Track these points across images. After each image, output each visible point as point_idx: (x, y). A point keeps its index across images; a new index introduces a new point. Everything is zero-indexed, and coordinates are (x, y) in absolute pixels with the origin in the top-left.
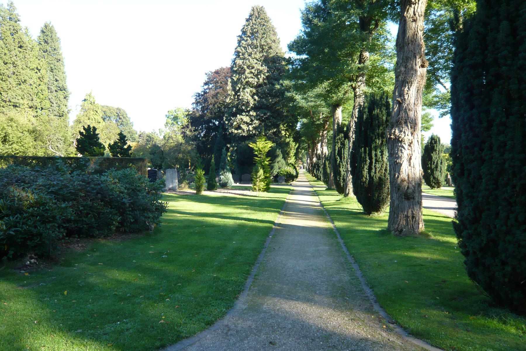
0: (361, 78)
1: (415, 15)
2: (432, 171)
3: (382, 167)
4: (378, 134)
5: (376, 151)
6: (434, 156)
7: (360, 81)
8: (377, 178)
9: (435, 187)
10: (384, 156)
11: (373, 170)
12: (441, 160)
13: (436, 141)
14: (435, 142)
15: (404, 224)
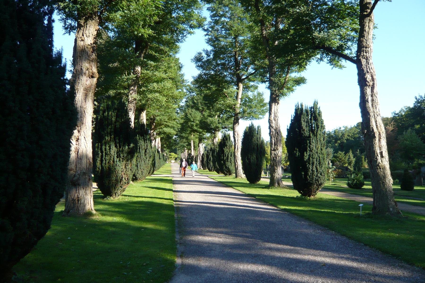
0: (133, 87)
1: (83, 35)
2: (225, 162)
3: (110, 159)
4: (107, 132)
5: (105, 146)
6: (226, 150)
7: (132, 90)
8: (107, 168)
9: (227, 175)
10: (111, 150)
11: (104, 162)
12: (231, 153)
13: (227, 138)
14: (226, 139)
15: (72, 206)
